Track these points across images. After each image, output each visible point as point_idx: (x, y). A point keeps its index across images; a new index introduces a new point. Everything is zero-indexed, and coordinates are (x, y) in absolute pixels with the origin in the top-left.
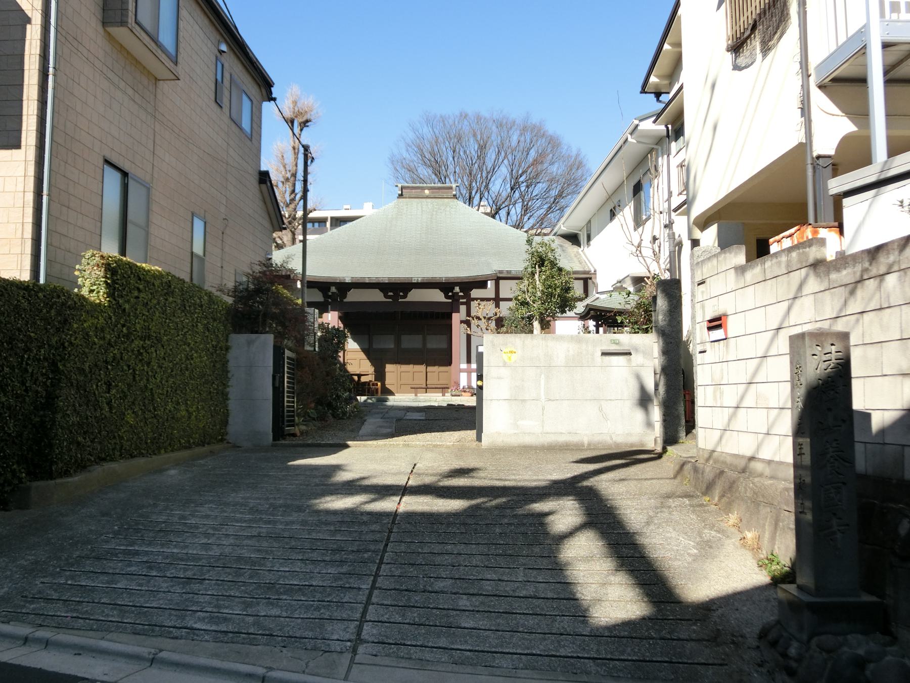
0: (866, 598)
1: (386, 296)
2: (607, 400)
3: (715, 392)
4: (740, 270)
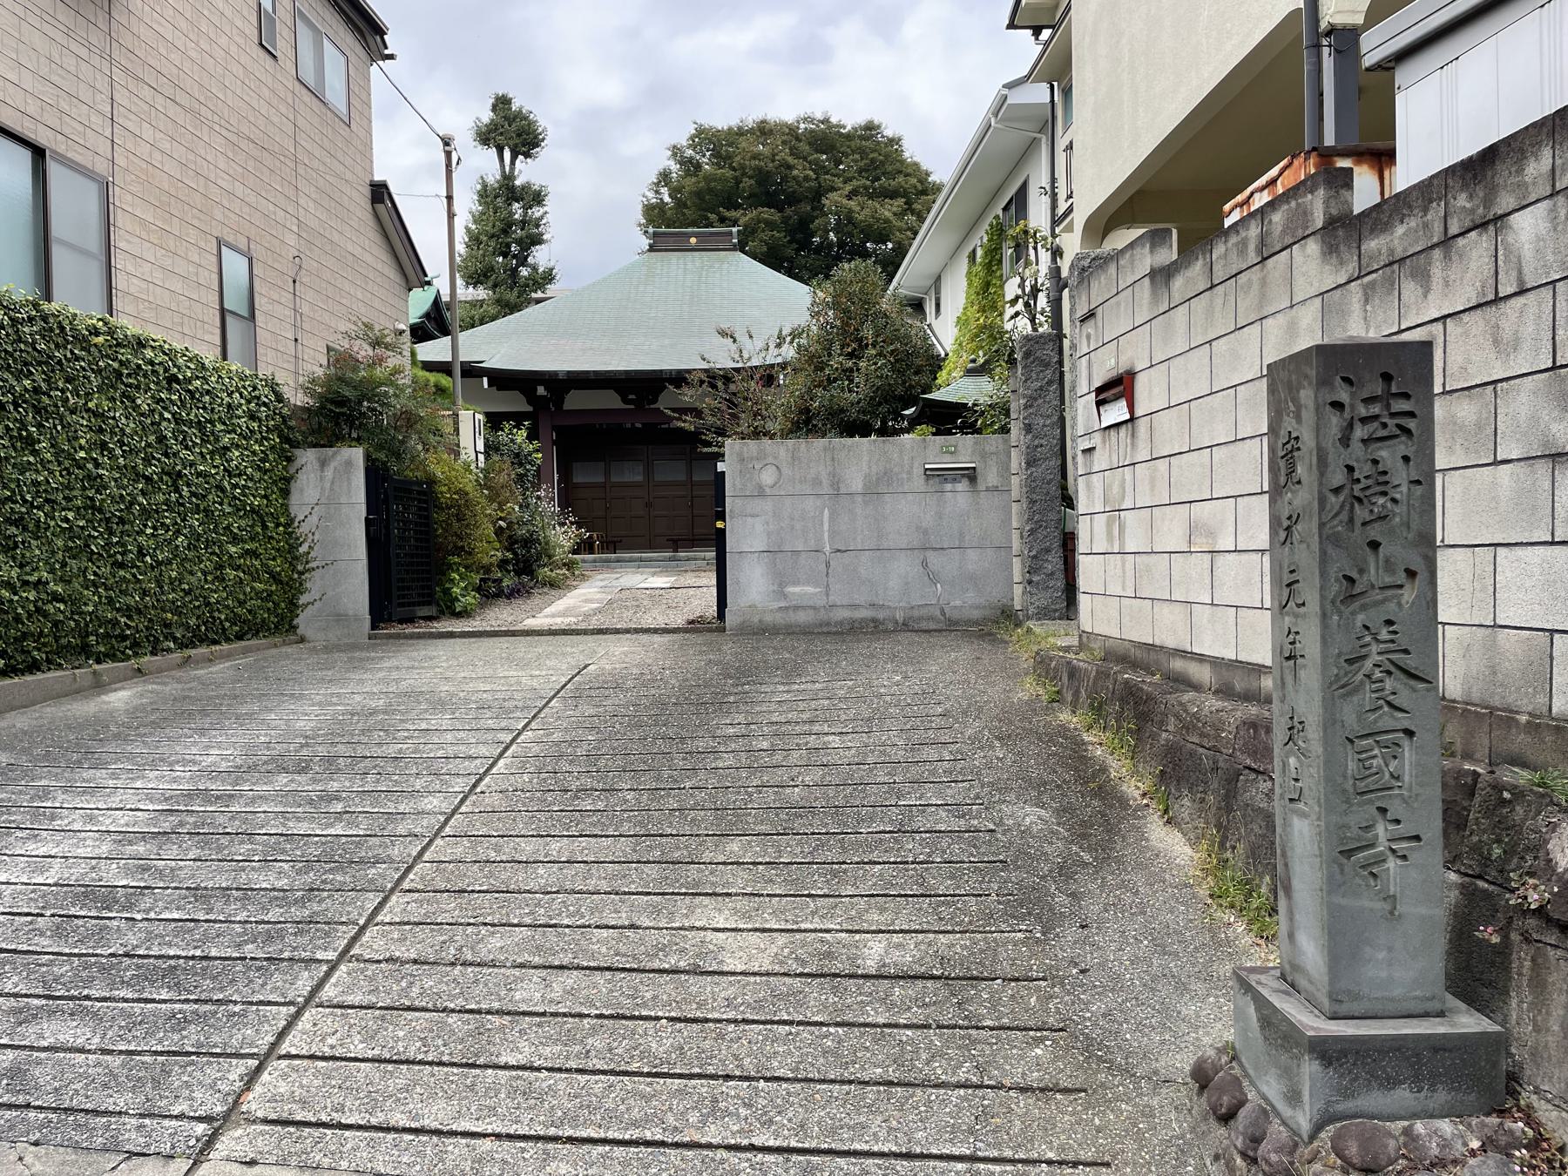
0: (1469, 1022)
1: (625, 401)
2: (935, 549)
3: (1109, 525)
4: (1161, 276)
